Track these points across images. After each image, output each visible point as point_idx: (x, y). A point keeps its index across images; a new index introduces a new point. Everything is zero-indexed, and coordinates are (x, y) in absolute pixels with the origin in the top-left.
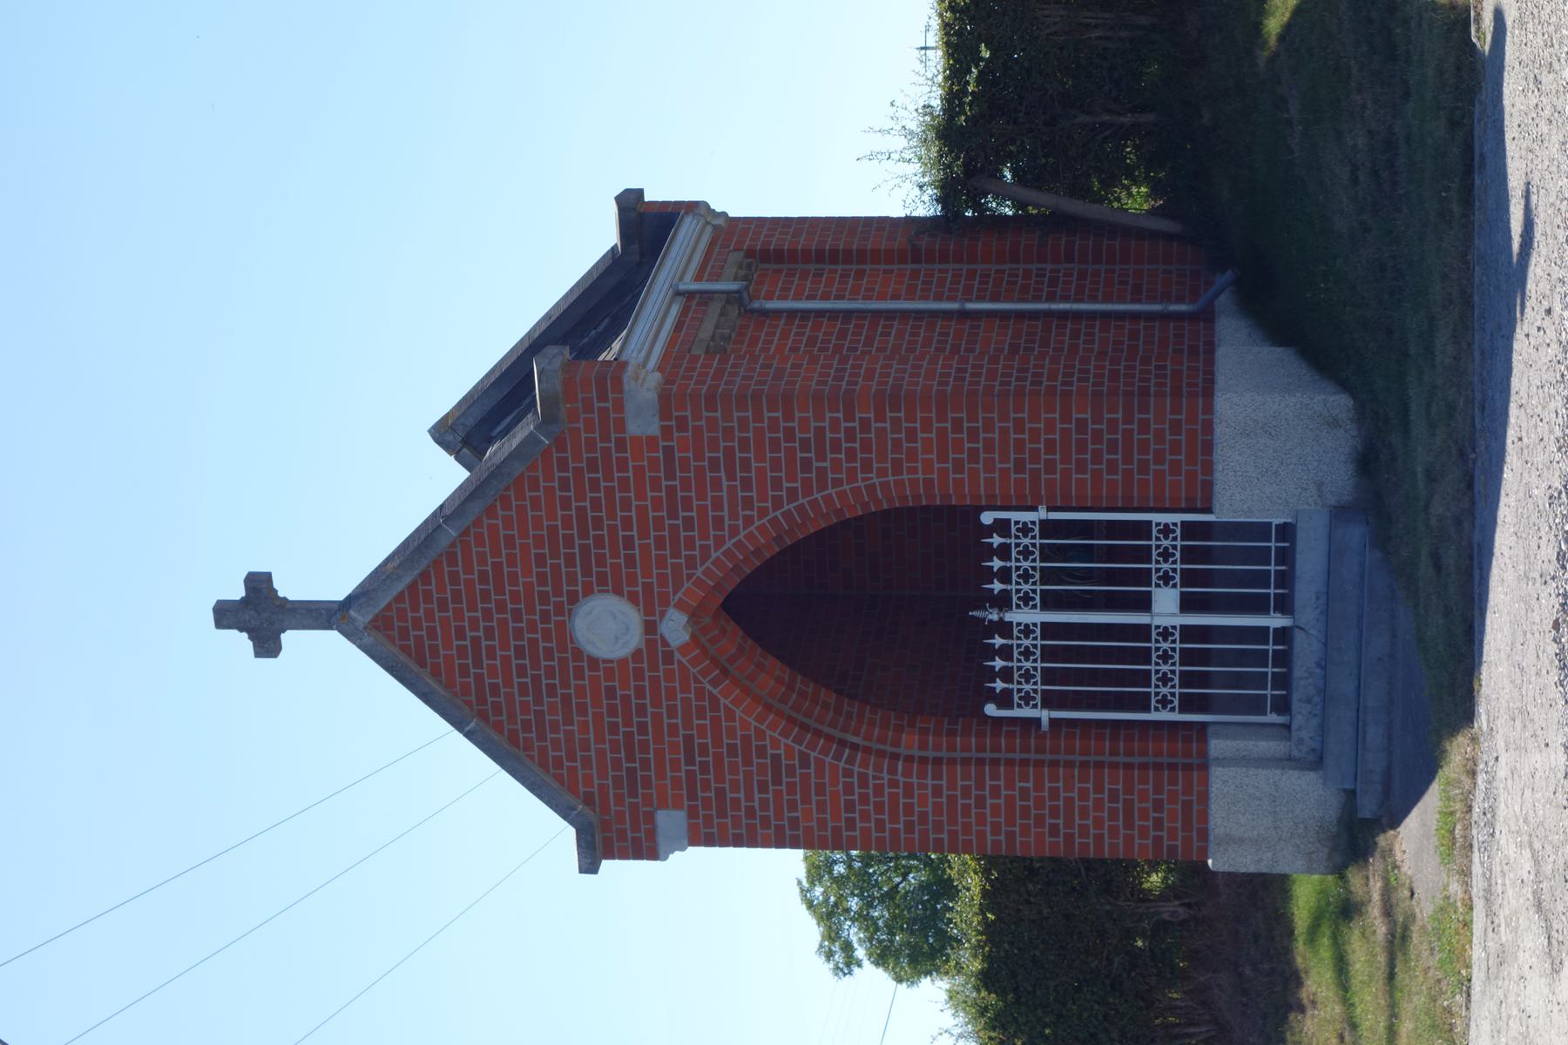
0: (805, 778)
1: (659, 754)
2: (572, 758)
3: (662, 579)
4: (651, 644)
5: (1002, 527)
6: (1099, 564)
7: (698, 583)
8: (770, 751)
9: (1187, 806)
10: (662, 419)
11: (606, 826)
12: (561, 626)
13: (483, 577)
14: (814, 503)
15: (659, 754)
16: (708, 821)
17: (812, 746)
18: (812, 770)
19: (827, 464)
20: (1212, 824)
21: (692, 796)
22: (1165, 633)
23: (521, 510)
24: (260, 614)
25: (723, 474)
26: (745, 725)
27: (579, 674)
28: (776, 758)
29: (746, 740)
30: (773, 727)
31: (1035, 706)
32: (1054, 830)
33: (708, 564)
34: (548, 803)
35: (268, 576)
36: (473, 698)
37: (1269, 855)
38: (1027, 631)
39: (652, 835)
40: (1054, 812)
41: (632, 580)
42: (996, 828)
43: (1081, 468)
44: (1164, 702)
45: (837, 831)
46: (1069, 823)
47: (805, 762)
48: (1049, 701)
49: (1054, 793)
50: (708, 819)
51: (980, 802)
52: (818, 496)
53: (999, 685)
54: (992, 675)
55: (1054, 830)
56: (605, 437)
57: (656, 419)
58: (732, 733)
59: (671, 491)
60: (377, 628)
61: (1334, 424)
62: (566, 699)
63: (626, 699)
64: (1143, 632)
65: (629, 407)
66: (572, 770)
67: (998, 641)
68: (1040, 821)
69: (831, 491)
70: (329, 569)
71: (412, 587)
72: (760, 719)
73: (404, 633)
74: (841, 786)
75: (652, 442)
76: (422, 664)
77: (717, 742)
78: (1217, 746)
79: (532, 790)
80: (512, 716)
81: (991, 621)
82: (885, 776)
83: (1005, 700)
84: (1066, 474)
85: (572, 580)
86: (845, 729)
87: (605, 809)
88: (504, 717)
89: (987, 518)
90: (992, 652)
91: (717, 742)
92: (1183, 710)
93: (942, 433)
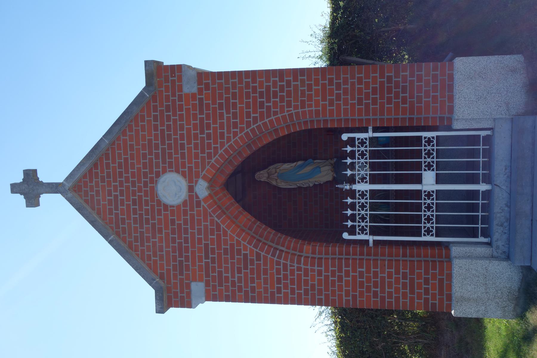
0: (259, 266)
1: (193, 253)
2: (155, 255)
3: (197, 164)
4: (191, 197)
5: (351, 142)
6: (397, 159)
7: (213, 166)
8: (243, 252)
9: (441, 281)
10: (199, 84)
11: (169, 290)
12: (152, 189)
13: (120, 165)
14: (265, 124)
15: (193, 253)
16: (214, 289)
17: (262, 249)
18: (262, 262)
19: (271, 104)
20: (454, 290)
21: (207, 275)
22: (429, 195)
23: (137, 131)
24: (30, 188)
25: (224, 111)
26: (232, 239)
27: (159, 212)
28: (245, 255)
29: (232, 245)
31: (366, 234)
32: (375, 294)
33: (217, 156)
34: (143, 277)
35: (35, 171)
36: (114, 226)
37: (483, 308)
38: (363, 195)
39: (189, 295)
40: (376, 285)
41: (184, 166)
42: (347, 295)
43: (389, 102)
44: (428, 232)
45: (273, 294)
46: (383, 291)
47: (258, 255)
48: (374, 231)
49: (376, 274)
50: (214, 287)
51: (340, 279)
52: (267, 120)
53: (350, 223)
55: (375, 294)
56: (174, 95)
57: (196, 85)
59: (202, 120)
60: (75, 191)
61: (514, 71)
62: (154, 225)
63: (179, 225)
64: (417, 194)
65: (184, 79)
66: (155, 262)
67: (349, 201)
68: (368, 289)
69: (273, 118)
70: (57, 168)
71: (90, 171)
72: (239, 235)
73: (86, 192)
74: (275, 270)
75: (194, 96)
76: (93, 209)
77: (219, 247)
78: (455, 251)
79: (136, 270)
80: (130, 235)
81: (346, 190)
83: (352, 231)
84: (368, 271)
85: (158, 166)
86: (278, 244)
87: (169, 282)
88: (127, 235)
89: (345, 137)
91: (219, 247)
93: (324, 85)
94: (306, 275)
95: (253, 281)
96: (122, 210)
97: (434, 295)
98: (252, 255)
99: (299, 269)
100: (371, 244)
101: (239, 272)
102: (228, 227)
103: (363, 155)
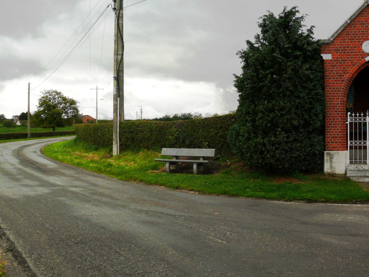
4: (365, 55)
9: (337, 147)
21: (335, 61)
22: (365, 143)
27: (359, 42)
28: (343, 76)
30: (349, 75)
44: (351, 143)
47: (343, 81)
48: (351, 124)
50: (330, 63)
51: (336, 111)
53: (353, 115)
54: (355, 113)
58: (348, 68)
67: (362, 115)
82: (340, 95)
90: (360, 113)
92: (350, 146)
94: (337, 99)
95: (333, 78)
96: (359, 27)
97: (331, 145)
98: (344, 78)
99: (339, 96)
100: (347, 123)
101: (337, 73)
102: (354, 69)
103: (356, 120)
